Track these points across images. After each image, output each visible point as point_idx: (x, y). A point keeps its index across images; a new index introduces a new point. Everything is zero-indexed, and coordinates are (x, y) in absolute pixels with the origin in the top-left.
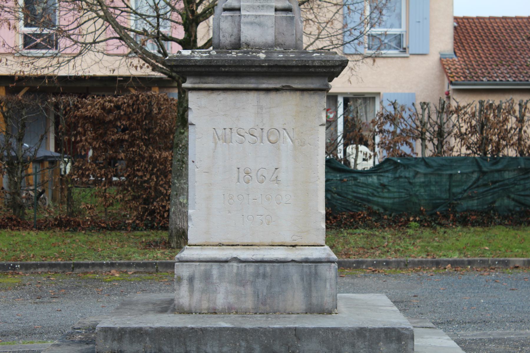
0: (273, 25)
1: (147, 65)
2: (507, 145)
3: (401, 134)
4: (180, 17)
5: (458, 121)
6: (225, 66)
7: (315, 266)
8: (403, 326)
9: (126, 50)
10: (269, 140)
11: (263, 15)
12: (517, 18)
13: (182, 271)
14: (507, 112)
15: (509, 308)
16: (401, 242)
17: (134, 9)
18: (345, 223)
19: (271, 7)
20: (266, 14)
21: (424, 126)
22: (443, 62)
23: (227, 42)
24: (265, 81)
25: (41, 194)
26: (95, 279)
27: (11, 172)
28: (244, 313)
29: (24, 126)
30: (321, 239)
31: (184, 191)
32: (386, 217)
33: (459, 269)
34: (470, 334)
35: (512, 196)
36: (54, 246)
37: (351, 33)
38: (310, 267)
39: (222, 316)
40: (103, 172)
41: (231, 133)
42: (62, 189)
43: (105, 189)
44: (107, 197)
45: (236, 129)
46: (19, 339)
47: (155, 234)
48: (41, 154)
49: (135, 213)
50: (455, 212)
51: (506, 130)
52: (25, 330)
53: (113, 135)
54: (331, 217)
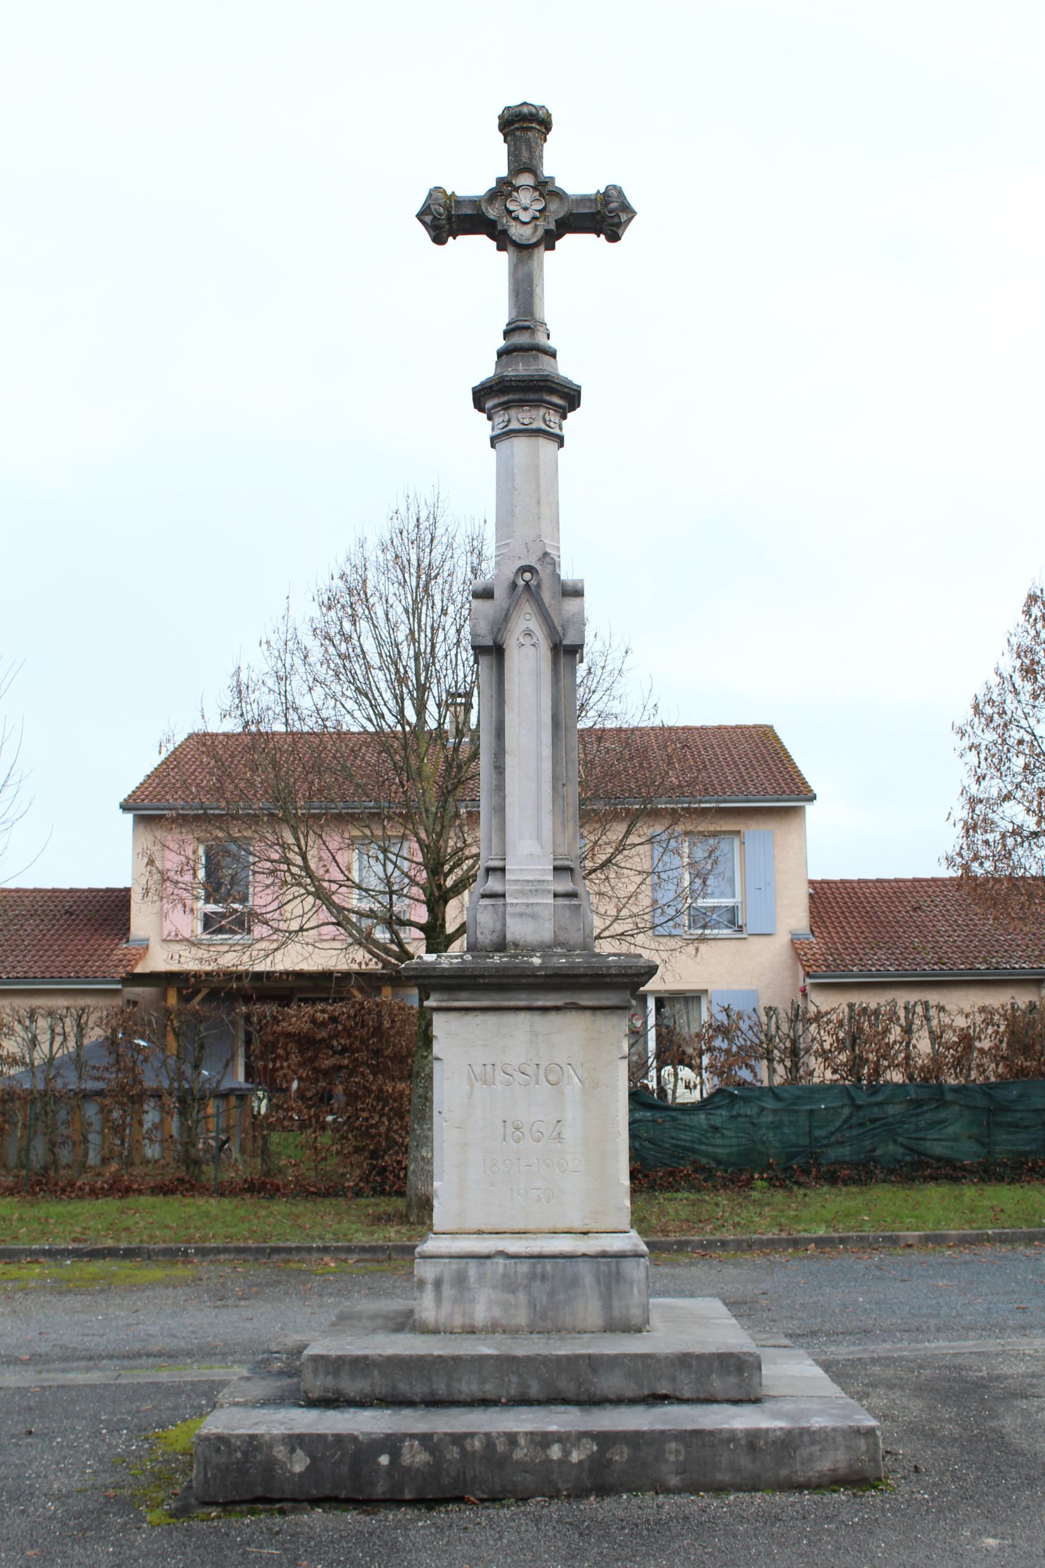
1: (374, 960)
2: (889, 1067)
5: (819, 1033)
6: (483, 977)
7: (617, 1263)
8: (745, 1350)
10: (548, 1081)
12: (897, 881)
13: (426, 1271)
14: (888, 1019)
15: (899, 1309)
17: (357, 881)
18: (661, 1184)
21: (771, 1040)
22: (796, 945)
23: (487, 941)
24: (541, 997)
25: (224, 1143)
27: (183, 1113)
28: (512, 1331)
29: (202, 1047)
31: (427, 1140)
32: (719, 1174)
33: (827, 1250)
34: (843, 1351)
35: (900, 1139)
36: (243, 1221)
38: (609, 1264)
40: (312, 1112)
41: (494, 1070)
42: (254, 1137)
43: (316, 1138)
46: (192, 1363)
48: (226, 1085)
49: (358, 1172)
50: (818, 1165)
51: (888, 1044)
52: (200, 1348)
54: (640, 1176)
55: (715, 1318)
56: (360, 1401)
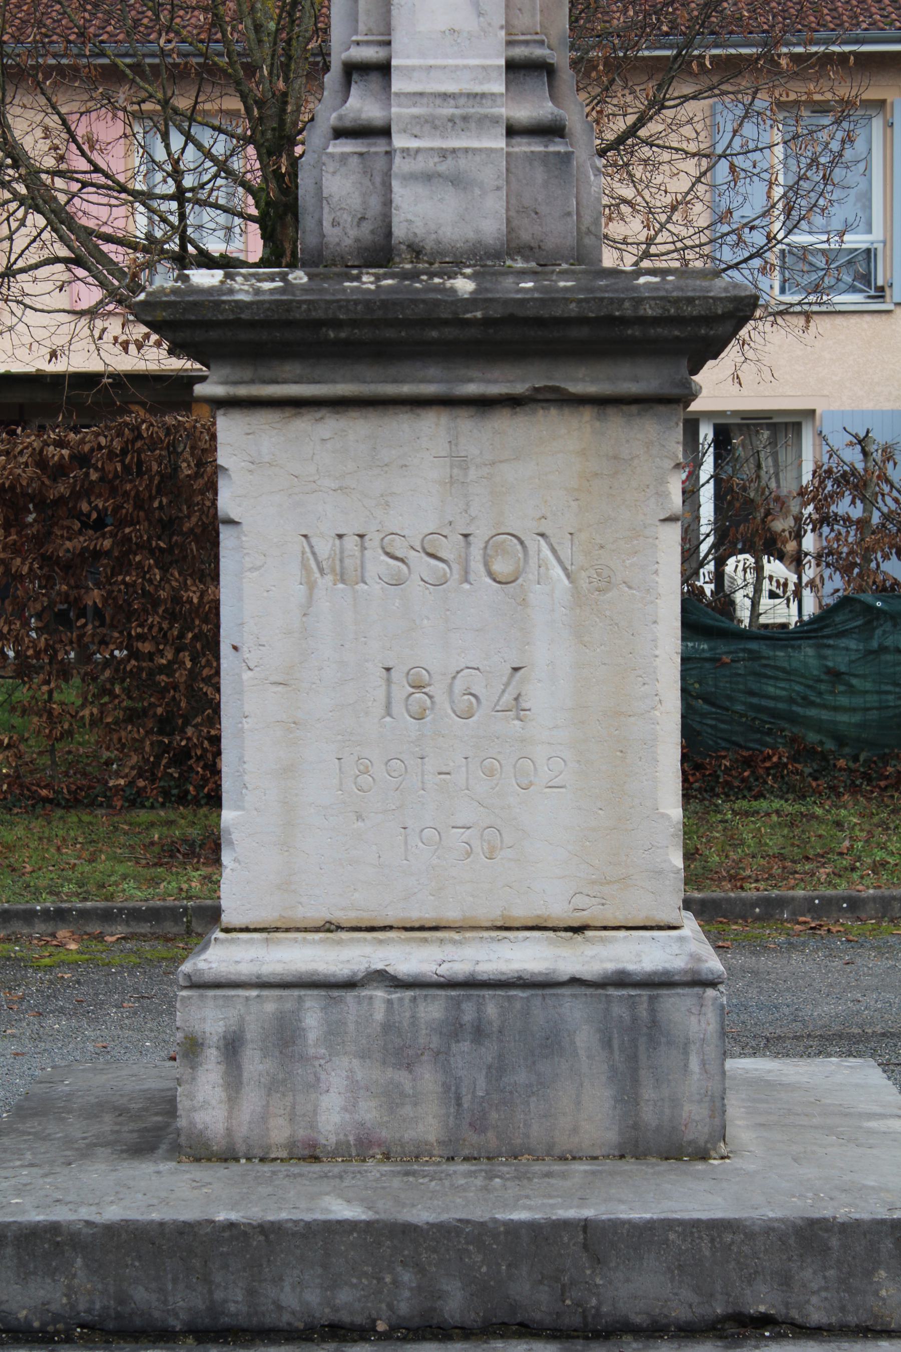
0: (502, 183)
3: (883, 525)
4: (251, 200)
6: (336, 324)
7: (651, 998)
9: (91, 295)
10: (491, 574)
11: (466, 150)
16: (890, 840)
18: (727, 783)
19: (495, 120)
20: (475, 144)
23: (348, 242)
24: (475, 374)
26: (9, 958)
28: (406, 1157)
30: (667, 900)
32: (842, 763)
37: (740, 238)
38: (632, 1003)
39: (336, 1170)
41: (363, 548)
44: (56, 713)
45: (377, 537)
47: (190, 818)
49: (134, 759)
53: (70, 539)
55: (871, 1116)
56: (42, 1330)
